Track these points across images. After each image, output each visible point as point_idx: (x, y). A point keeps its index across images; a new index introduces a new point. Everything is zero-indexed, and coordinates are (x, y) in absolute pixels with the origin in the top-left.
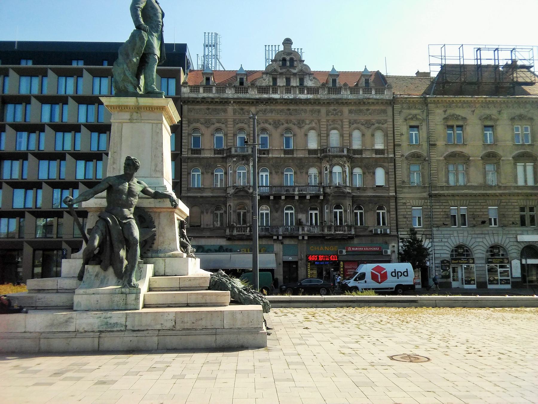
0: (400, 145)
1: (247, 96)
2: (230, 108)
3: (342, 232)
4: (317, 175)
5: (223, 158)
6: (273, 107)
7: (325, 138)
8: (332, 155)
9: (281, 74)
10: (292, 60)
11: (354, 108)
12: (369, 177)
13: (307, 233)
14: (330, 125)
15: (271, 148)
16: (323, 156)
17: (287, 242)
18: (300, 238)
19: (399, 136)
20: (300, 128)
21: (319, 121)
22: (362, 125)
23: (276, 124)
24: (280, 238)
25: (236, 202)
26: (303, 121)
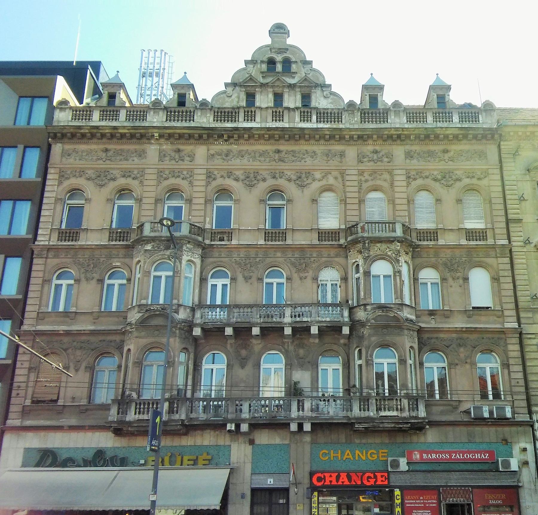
0: (520, 221)
1: (193, 124)
2: (152, 150)
3: (395, 413)
4: (339, 283)
5: (127, 247)
6: (245, 148)
7: (356, 207)
8: (368, 238)
9: (262, 85)
10: (287, 63)
11: (416, 148)
12: (455, 287)
13: (310, 414)
14: (366, 181)
15: (236, 226)
16: (350, 241)
17: (264, 438)
18: (294, 427)
19: (522, 244)
20: (302, 186)
21: (343, 174)
22: (435, 180)
23: (251, 180)
24: (244, 427)
25: (143, 341)
26: (308, 174)
